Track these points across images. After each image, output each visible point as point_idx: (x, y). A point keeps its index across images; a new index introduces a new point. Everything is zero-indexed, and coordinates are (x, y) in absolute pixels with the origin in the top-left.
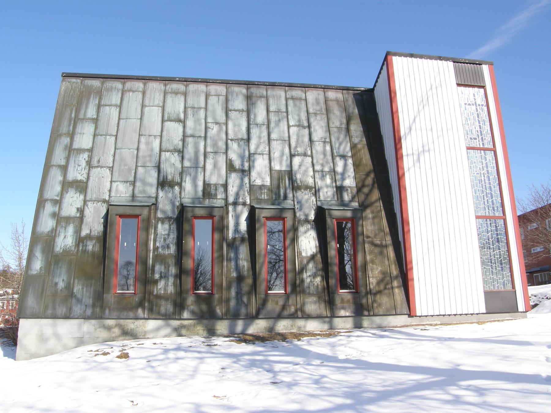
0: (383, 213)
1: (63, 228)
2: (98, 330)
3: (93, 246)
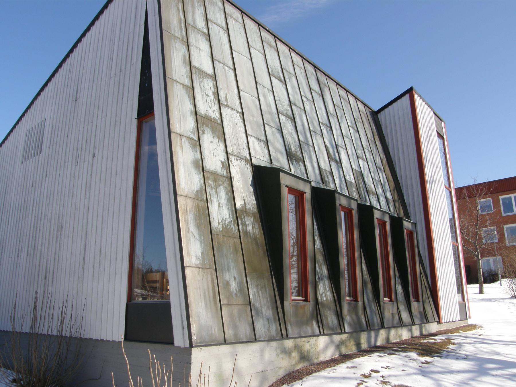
0: (325, 188)
1: (214, 190)
2: (281, 356)
3: (252, 226)
